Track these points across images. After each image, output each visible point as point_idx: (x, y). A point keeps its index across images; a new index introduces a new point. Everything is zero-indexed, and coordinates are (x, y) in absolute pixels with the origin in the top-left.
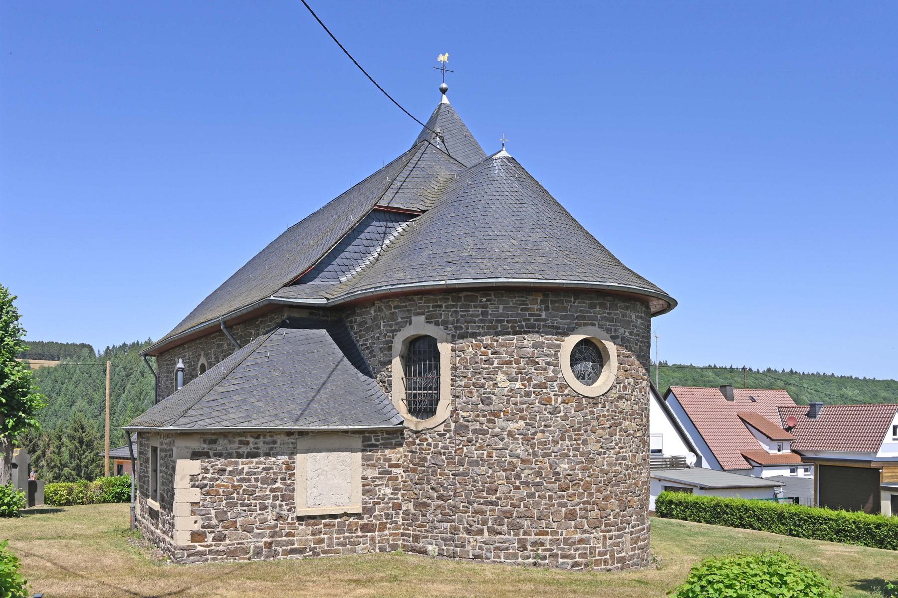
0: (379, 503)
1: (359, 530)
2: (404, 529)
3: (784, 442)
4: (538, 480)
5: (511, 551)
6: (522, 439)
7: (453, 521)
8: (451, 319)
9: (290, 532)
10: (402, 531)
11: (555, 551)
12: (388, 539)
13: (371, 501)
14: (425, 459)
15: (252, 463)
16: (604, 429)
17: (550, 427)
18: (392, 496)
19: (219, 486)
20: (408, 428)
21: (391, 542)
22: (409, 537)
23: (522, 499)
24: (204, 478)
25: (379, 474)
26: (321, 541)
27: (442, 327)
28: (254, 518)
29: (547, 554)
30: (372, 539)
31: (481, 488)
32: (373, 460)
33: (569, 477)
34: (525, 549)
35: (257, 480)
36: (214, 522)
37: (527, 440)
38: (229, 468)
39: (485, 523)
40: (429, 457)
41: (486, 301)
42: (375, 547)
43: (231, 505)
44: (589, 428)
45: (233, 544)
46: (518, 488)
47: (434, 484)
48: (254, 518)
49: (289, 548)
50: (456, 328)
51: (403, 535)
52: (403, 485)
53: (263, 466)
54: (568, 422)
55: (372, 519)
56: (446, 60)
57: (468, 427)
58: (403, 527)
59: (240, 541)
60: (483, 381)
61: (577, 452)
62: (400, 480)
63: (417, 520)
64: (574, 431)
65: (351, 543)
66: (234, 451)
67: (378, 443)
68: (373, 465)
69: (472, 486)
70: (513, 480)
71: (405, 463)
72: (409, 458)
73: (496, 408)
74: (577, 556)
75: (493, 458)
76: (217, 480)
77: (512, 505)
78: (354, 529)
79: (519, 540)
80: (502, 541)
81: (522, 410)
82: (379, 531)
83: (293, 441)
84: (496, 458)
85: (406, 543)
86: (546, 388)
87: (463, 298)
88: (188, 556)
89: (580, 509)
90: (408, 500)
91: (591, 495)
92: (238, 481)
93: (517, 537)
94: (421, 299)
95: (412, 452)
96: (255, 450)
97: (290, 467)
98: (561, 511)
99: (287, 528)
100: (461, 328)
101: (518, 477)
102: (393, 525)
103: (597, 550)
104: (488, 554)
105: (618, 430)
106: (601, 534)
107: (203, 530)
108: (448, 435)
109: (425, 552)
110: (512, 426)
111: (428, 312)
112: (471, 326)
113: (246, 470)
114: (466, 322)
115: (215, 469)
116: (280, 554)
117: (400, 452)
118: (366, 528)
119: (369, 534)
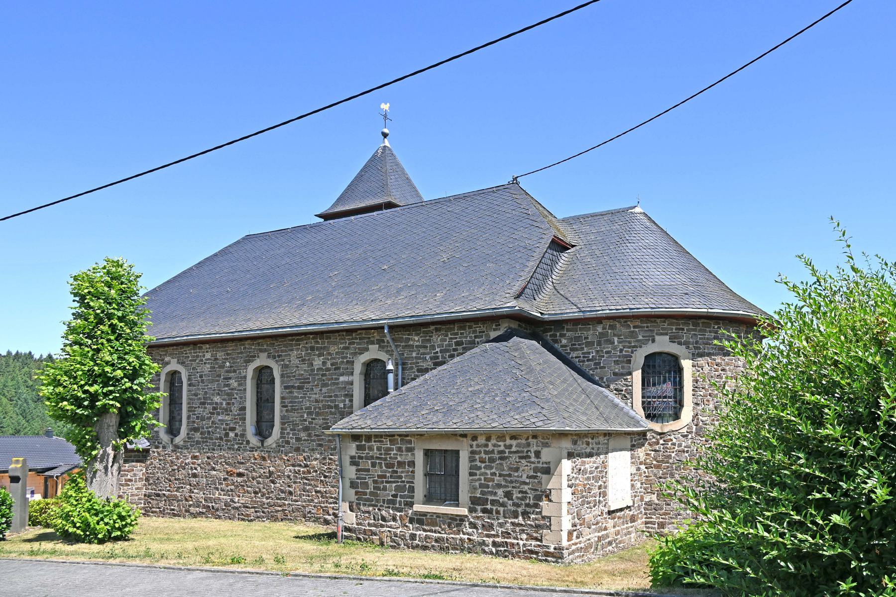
2: (646, 518)
8: (691, 340)
14: (669, 457)
20: (652, 430)
22: (655, 524)
27: (684, 347)
40: (673, 455)
47: (677, 477)
56: (387, 109)
63: (662, 509)
71: (648, 461)
72: (652, 456)
87: (701, 324)
90: (651, 493)
94: (665, 322)
95: (655, 451)
97: (604, 464)
100: (700, 348)
108: (690, 436)
111: (671, 333)
112: (707, 347)
114: (704, 343)
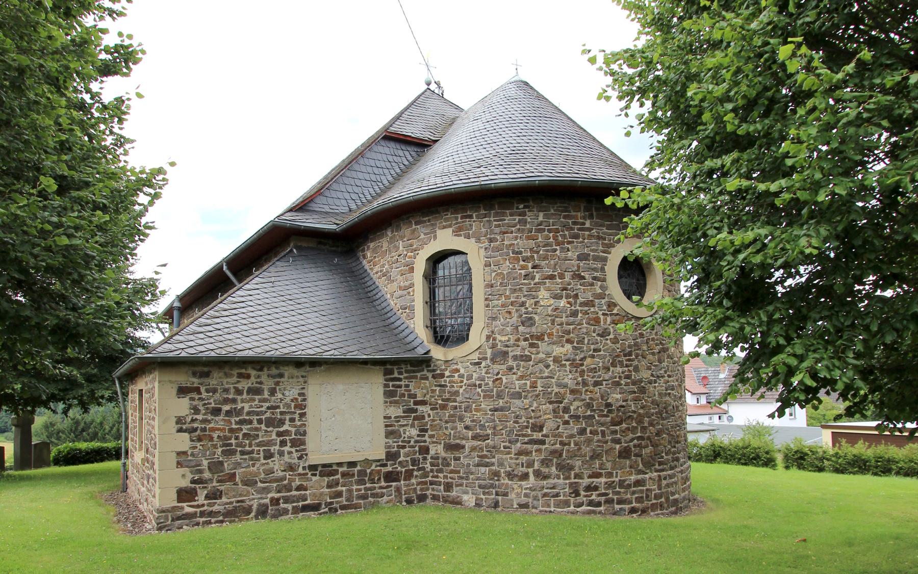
0: (404, 447)
1: (382, 479)
2: (433, 477)
3: (702, 396)
4: (589, 413)
5: (561, 498)
6: (570, 365)
7: (493, 464)
8: (483, 230)
9: (301, 485)
10: (430, 478)
11: (610, 496)
12: (415, 489)
13: (395, 444)
15: (254, 400)
16: (653, 354)
17: (600, 351)
18: (419, 438)
19: (213, 430)
21: (419, 493)
23: (572, 436)
24: (193, 421)
25: (404, 412)
26: (339, 494)
27: (473, 240)
28: (259, 468)
29: (603, 499)
30: (398, 490)
31: (525, 424)
32: (396, 397)
33: (622, 409)
34: (577, 494)
35: (260, 422)
36: (207, 475)
37: (576, 365)
38: (226, 408)
39: (530, 464)
40: (461, 391)
41: (524, 208)
42: (401, 498)
43: (229, 453)
44: (640, 352)
45: (231, 503)
46: (567, 423)
47: (468, 422)
48: (259, 468)
49: (300, 504)
50: (491, 240)
51: (432, 483)
52: (431, 425)
53: (267, 404)
54: (618, 345)
55: (397, 466)
57: (508, 353)
58: (431, 474)
59: (239, 499)
60: (523, 299)
61: (629, 381)
62: (427, 419)
64: (625, 355)
65: (373, 495)
66: (232, 386)
67: (401, 377)
68: (396, 402)
69: (515, 422)
70: (561, 414)
72: (438, 393)
73: (539, 330)
74: (634, 501)
75: (538, 389)
76: (209, 422)
77: (562, 443)
78: (376, 478)
79: (571, 484)
80: (552, 486)
81: (568, 332)
82: (405, 480)
83: (304, 374)
84: (541, 389)
85: (435, 493)
86: (594, 306)
88: (173, 520)
89: (635, 446)
91: (644, 429)
92: (237, 423)
93: (568, 481)
96: (257, 385)
98: (615, 449)
99: (297, 480)
101: (566, 410)
102: (420, 472)
103: (653, 492)
104: (535, 502)
105: (666, 357)
106: (656, 474)
107: (193, 485)
108: (483, 364)
109: (457, 502)
110: (558, 351)
112: (507, 237)
113: (246, 409)
115: (207, 408)
116: (290, 512)
117: (426, 387)
118: (391, 477)
119: (394, 484)
